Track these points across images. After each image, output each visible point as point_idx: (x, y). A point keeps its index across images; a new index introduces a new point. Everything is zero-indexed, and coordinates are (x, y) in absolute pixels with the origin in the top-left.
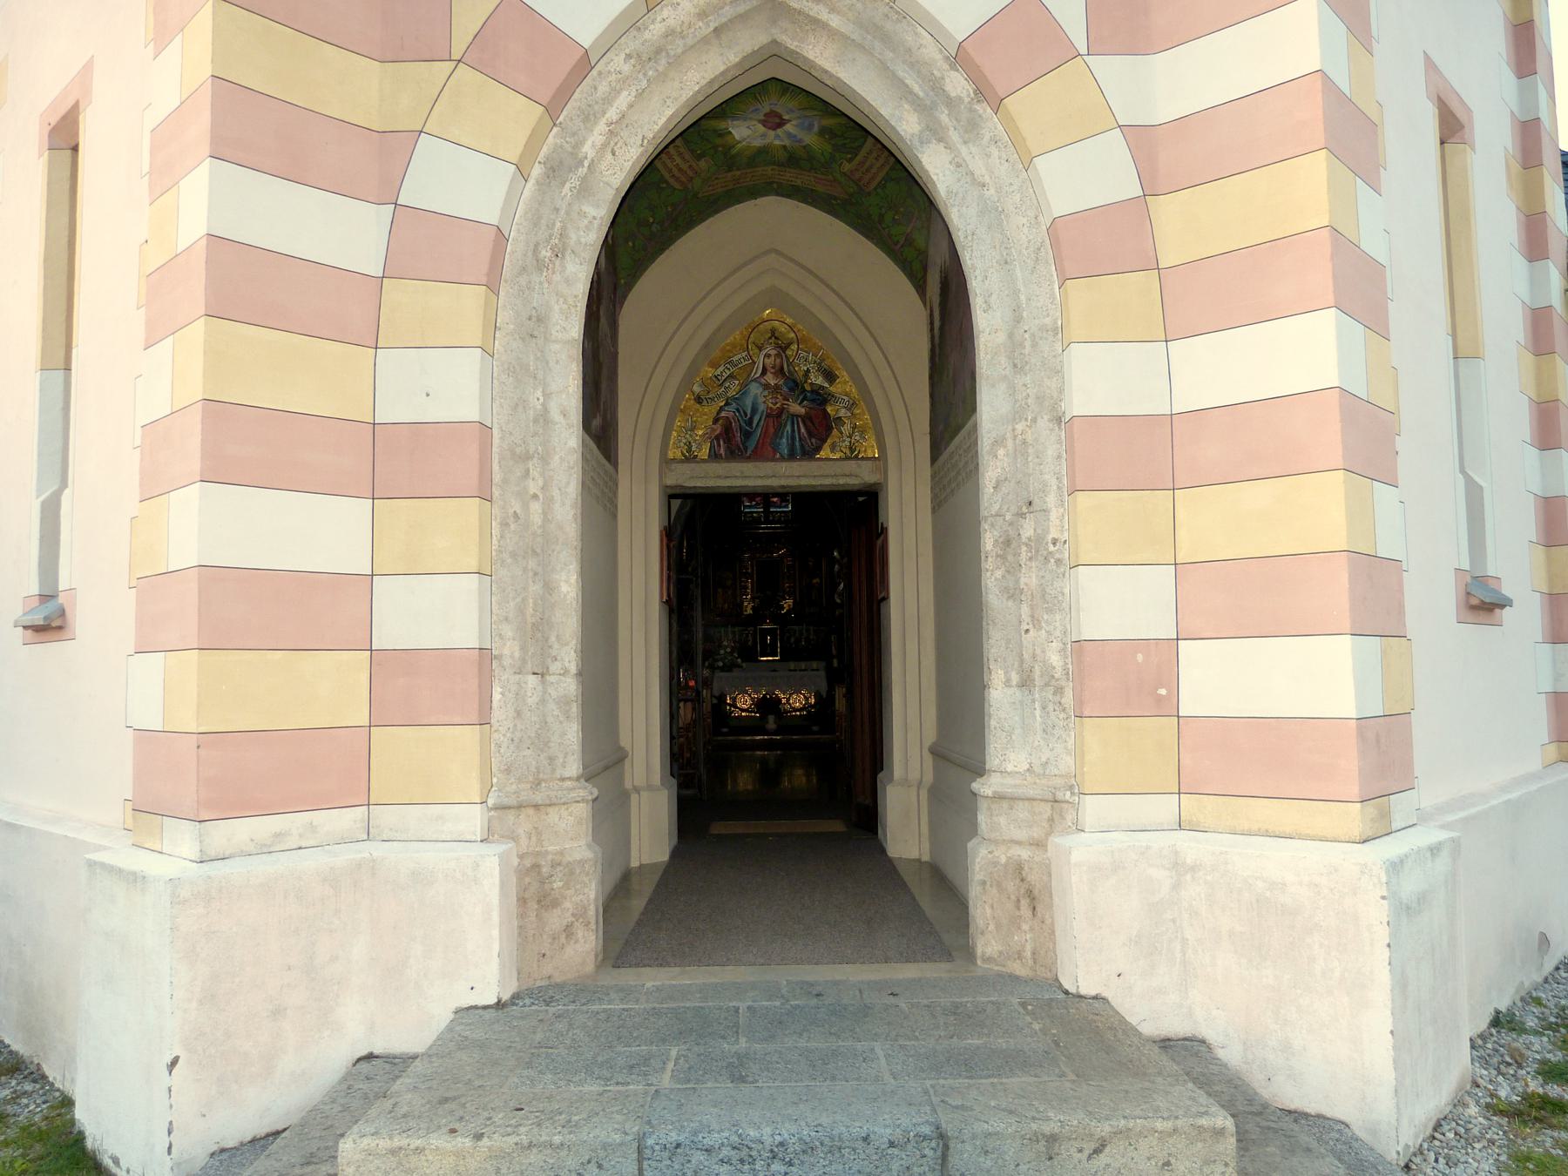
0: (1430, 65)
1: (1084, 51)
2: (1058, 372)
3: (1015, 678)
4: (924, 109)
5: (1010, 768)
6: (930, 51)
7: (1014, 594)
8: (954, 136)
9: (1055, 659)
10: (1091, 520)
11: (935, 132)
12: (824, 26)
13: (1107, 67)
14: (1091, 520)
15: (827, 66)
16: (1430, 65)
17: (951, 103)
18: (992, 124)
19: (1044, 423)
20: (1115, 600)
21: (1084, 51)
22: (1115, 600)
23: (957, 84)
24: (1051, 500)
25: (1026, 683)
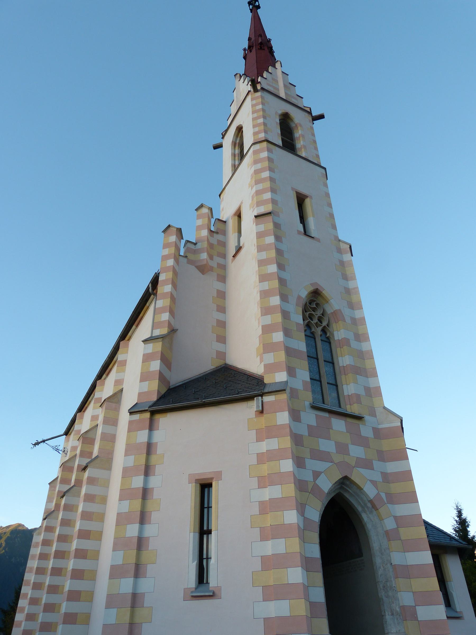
0: (242, 203)
1: (309, 491)
2: (390, 556)
3: (390, 614)
4: (362, 507)
5: (392, 632)
6: (365, 499)
7: (388, 597)
8: (368, 513)
9: (398, 610)
10: (401, 582)
11: (365, 512)
12: (349, 492)
13: (389, 506)
14: (401, 582)
15: (348, 497)
16: (242, 203)
17: (368, 507)
18: (375, 512)
19: (389, 565)
20: (406, 599)
21: (309, 491)
22: (406, 599)
23: (369, 505)
24: (392, 579)
25: (392, 614)
